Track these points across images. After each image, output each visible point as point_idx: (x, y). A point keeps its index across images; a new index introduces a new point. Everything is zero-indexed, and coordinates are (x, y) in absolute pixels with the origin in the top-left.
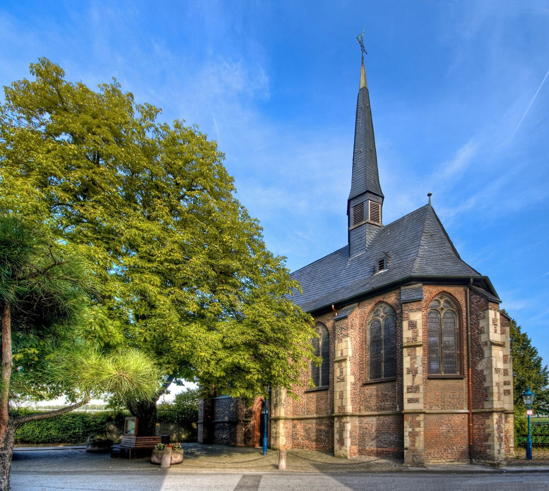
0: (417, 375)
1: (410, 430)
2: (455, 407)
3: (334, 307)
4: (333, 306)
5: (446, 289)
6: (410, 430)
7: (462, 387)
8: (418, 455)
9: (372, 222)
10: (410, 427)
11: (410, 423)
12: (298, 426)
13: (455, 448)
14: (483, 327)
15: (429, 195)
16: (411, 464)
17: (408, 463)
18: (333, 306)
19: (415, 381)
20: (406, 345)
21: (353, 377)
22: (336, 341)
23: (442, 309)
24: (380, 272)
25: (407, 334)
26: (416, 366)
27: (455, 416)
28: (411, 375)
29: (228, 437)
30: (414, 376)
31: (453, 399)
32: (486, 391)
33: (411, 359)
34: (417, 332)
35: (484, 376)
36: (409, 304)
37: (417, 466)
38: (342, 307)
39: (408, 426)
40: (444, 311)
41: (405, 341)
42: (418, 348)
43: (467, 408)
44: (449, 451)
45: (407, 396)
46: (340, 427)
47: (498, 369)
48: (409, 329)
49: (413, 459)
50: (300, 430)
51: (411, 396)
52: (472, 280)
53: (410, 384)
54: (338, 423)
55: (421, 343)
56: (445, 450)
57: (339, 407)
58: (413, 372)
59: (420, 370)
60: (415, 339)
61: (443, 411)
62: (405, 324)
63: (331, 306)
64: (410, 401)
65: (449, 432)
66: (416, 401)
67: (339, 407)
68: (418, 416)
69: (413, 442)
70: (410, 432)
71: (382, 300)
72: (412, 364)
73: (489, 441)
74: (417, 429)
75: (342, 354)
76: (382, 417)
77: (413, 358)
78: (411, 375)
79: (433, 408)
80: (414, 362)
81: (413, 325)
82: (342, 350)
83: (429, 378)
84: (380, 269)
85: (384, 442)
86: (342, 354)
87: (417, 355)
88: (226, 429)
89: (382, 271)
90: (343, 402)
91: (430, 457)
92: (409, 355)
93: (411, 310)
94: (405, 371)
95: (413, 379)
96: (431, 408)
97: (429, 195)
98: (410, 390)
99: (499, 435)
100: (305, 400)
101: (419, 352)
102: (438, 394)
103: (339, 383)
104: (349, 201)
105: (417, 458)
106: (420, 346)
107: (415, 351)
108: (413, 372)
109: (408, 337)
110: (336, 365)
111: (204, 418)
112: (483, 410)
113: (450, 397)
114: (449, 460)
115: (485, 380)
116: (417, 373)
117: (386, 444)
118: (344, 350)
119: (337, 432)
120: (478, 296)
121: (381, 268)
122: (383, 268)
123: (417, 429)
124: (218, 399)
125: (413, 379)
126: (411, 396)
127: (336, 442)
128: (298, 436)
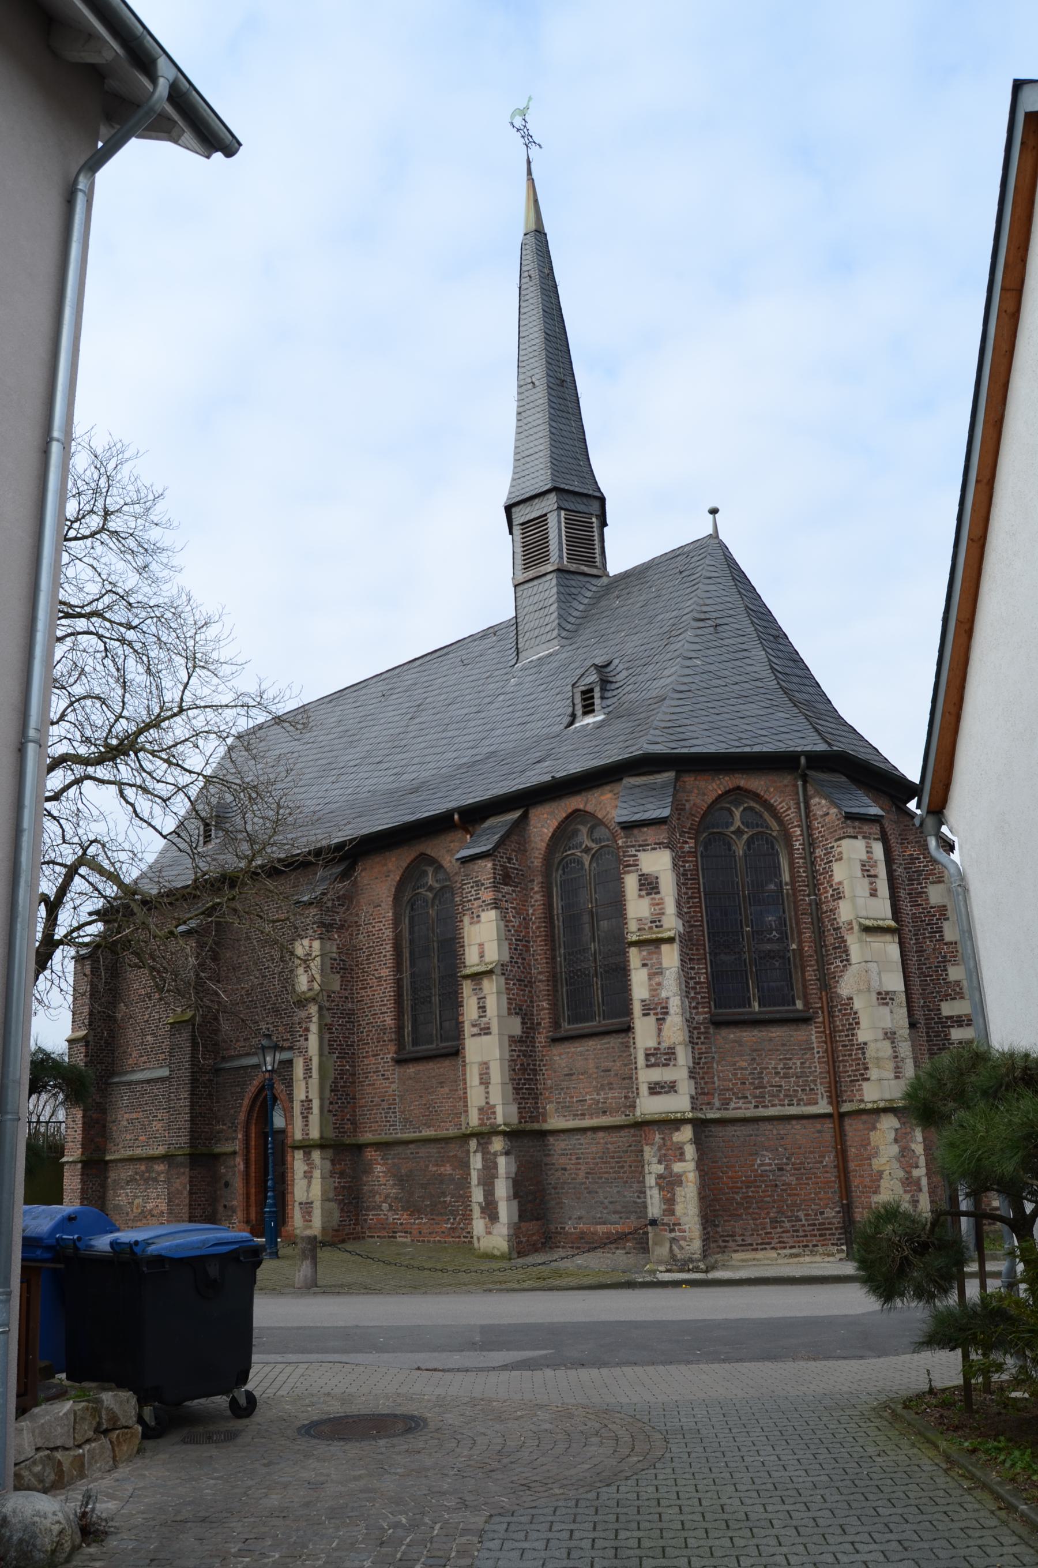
0: (669, 1019)
1: (660, 1169)
2: (791, 1098)
3: (460, 818)
4: (456, 817)
5: (742, 781)
6: (660, 1169)
7: (809, 1042)
8: (684, 1239)
9: (573, 567)
10: (660, 1162)
11: (660, 1149)
12: (379, 1168)
13: (801, 1214)
14: (840, 883)
15: (714, 511)
16: (667, 1263)
17: (660, 1262)
18: (456, 817)
19: (664, 1033)
20: (634, 938)
21: (518, 1020)
22: (466, 920)
23: (739, 832)
24: (585, 722)
25: (637, 908)
26: (664, 995)
27: (797, 1125)
28: (652, 1019)
29: (164, 1207)
30: (660, 1021)
31: (786, 1076)
32: (864, 1053)
33: (651, 976)
34: (660, 903)
35: (856, 1013)
36: (636, 831)
37: (681, 1271)
38: (484, 819)
39: (655, 1160)
40: (745, 837)
41: (632, 926)
42: (665, 948)
43: (825, 1101)
44: (787, 1225)
45: (646, 1076)
46: (485, 1167)
47: (887, 993)
48: (640, 896)
49: (671, 1250)
50: (383, 1180)
51: (656, 1075)
52: (803, 760)
53: (652, 1043)
54: (479, 1156)
55: (671, 934)
56: (775, 1222)
57: (481, 1110)
58: (658, 1010)
59: (675, 1004)
60: (656, 922)
61: (762, 1112)
62: (631, 882)
63: (453, 816)
64: (656, 1089)
65: (781, 1169)
66: (671, 1088)
67: (481, 1110)
68: (678, 1129)
69: (670, 1202)
70: (660, 1177)
71: (581, 807)
72: (654, 990)
73: (882, 1189)
74: (678, 1167)
75: (482, 956)
76: (601, 1134)
77: (656, 973)
78: (652, 1019)
79: (732, 1105)
80: (659, 984)
81: (649, 885)
82: (481, 945)
83: (718, 1023)
84: (585, 713)
85: (610, 1206)
86: (482, 956)
87: (665, 965)
88: (155, 1180)
89: (590, 720)
90: (484, 1095)
91: (731, 1244)
92: (644, 965)
93: (643, 847)
94: (637, 1008)
95: (660, 1030)
96: (725, 1104)
97: (714, 511)
98: (653, 1060)
99: (909, 1173)
100: (394, 1086)
101: (671, 957)
102: (744, 1064)
103: (478, 1039)
104: (509, 509)
105: (681, 1248)
106: (670, 940)
107: (660, 953)
108: (658, 1010)
109: (639, 916)
110: (467, 987)
111: (84, 1146)
112: (862, 1106)
113: (777, 1073)
114: (788, 1251)
115: (858, 1023)
116: (667, 1013)
117: (615, 1212)
118: (486, 945)
119: (479, 1184)
120: (823, 802)
121: (589, 709)
122: (593, 711)
123: (678, 1167)
124: (130, 1083)
125: (660, 1030)
126: (656, 1075)
127: (476, 1212)
128: (377, 1198)
